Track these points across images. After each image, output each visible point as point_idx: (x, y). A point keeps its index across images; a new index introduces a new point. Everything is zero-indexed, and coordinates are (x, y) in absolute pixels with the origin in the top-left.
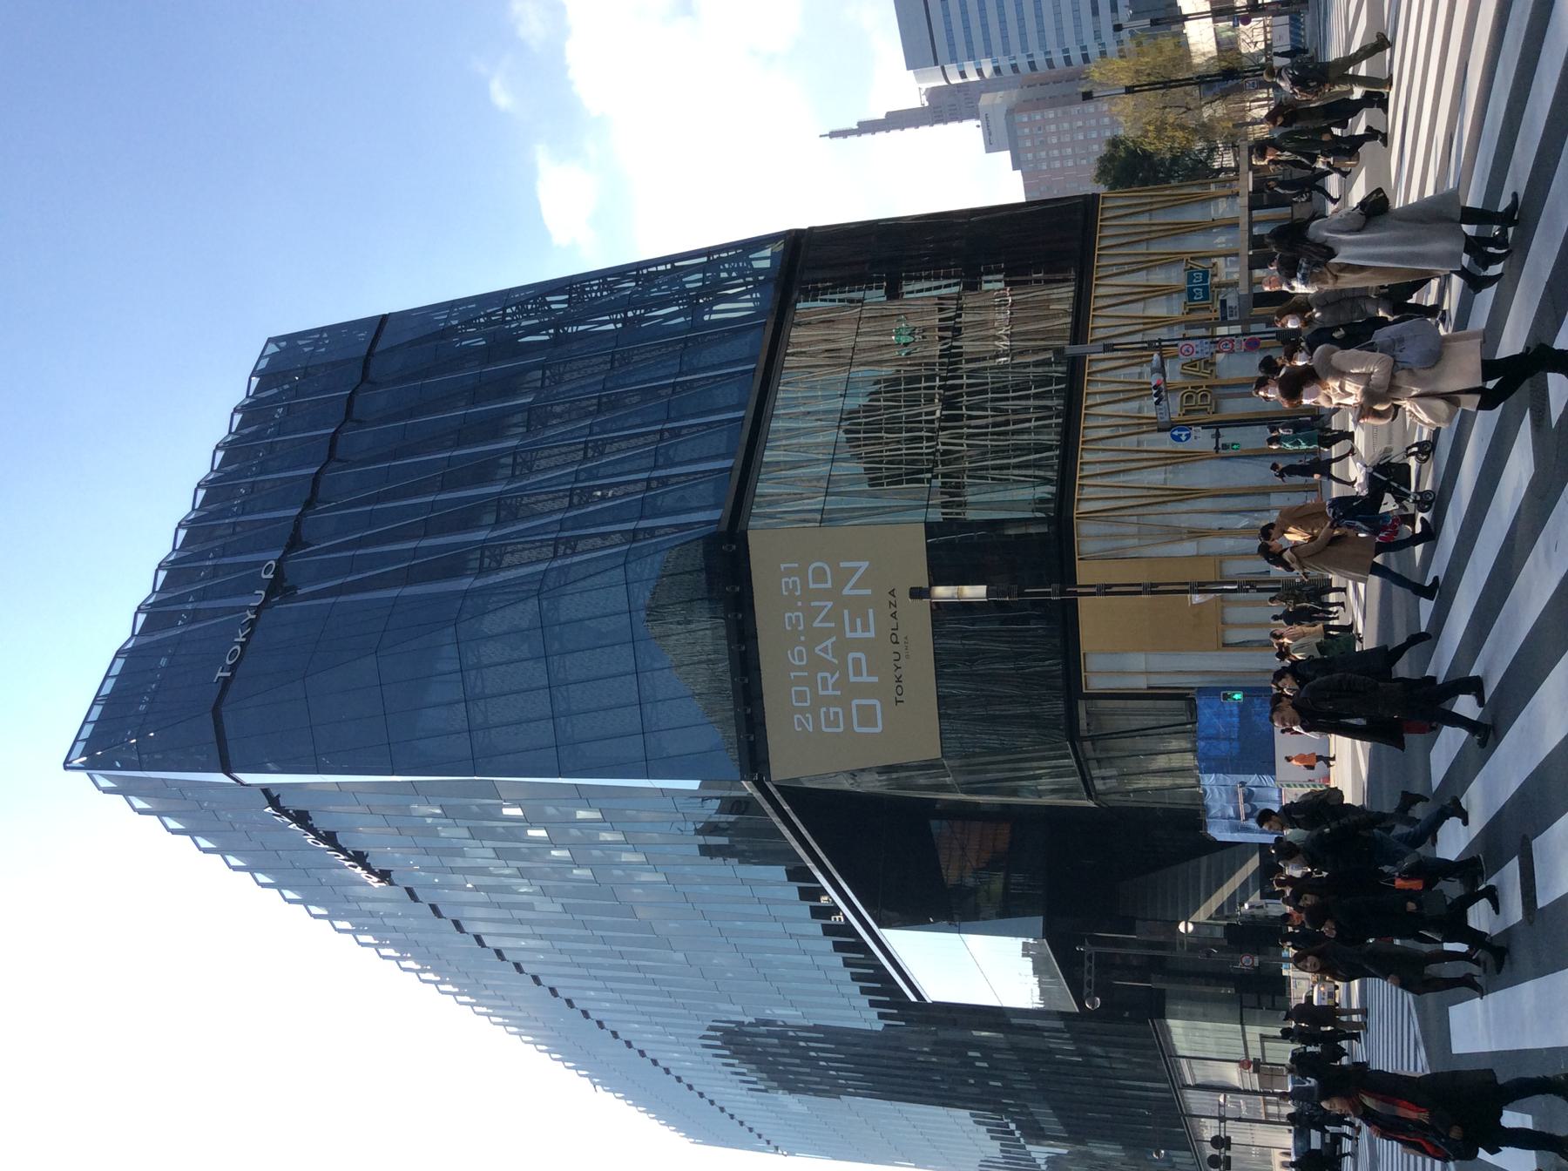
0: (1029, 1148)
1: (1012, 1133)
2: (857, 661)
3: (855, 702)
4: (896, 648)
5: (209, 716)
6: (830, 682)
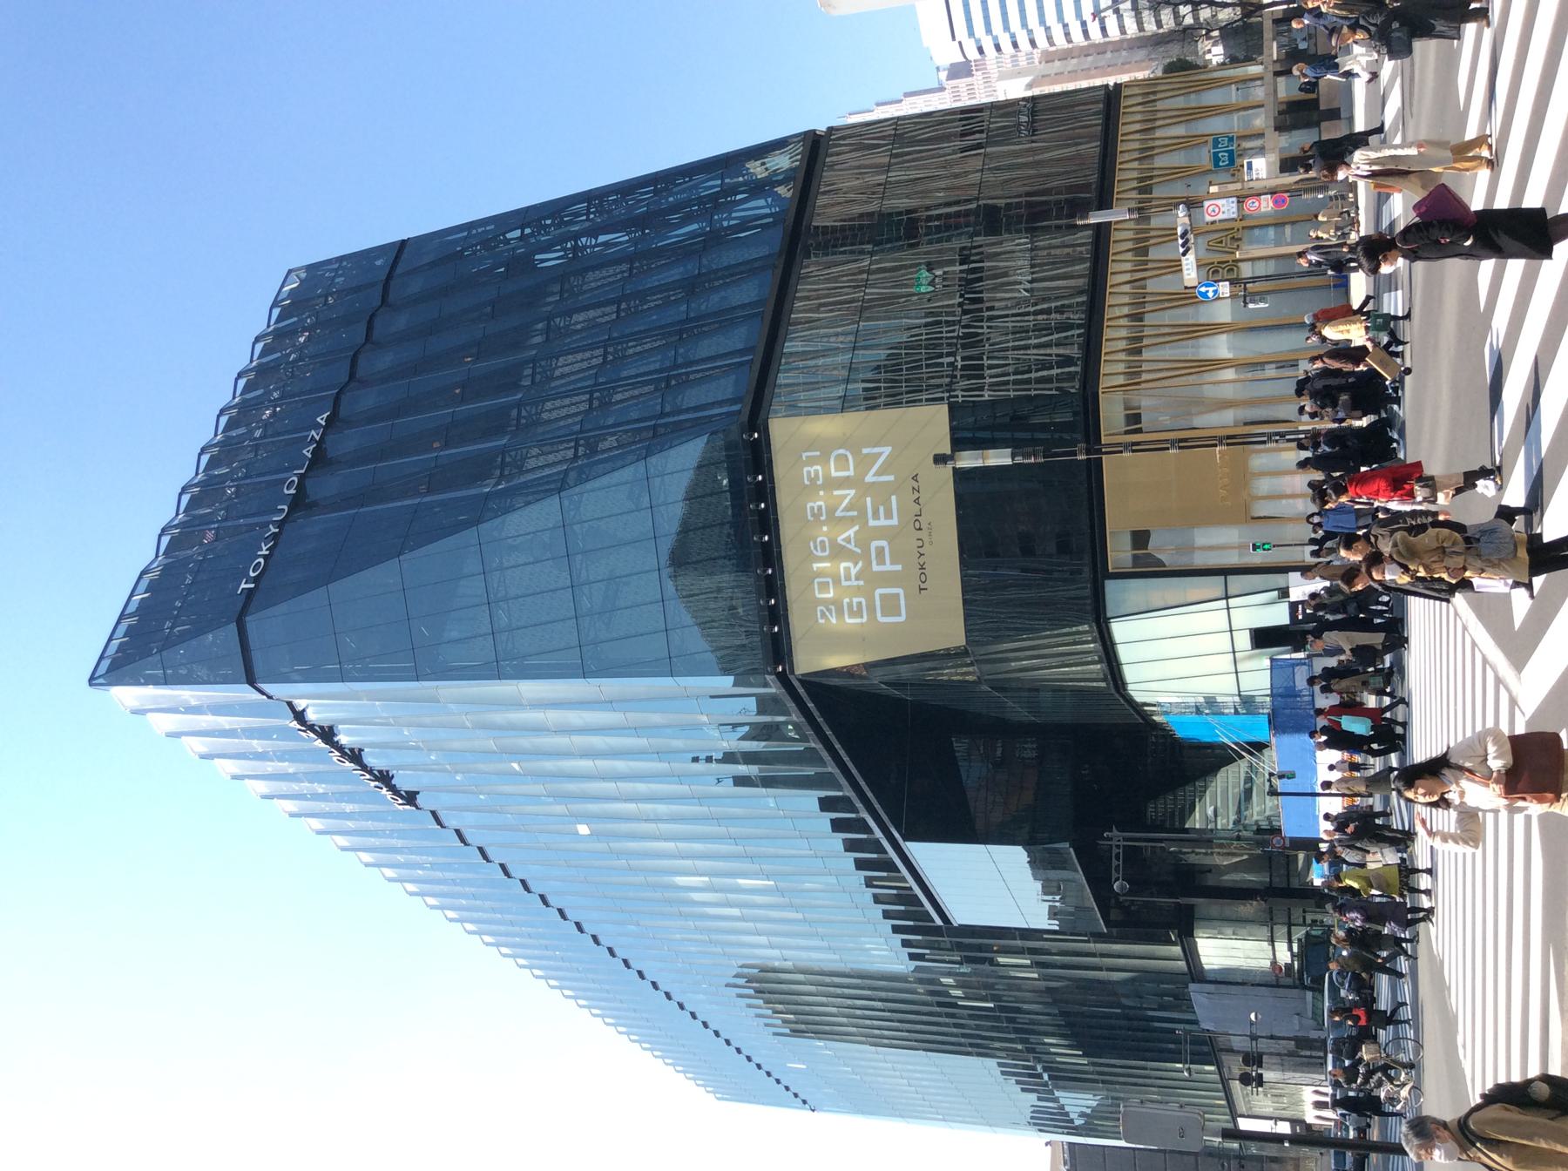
0: (1057, 1094)
1: (1040, 1076)
2: (880, 551)
3: (879, 592)
4: (919, 534)
5: (233, 627)
6: (854, 572)
